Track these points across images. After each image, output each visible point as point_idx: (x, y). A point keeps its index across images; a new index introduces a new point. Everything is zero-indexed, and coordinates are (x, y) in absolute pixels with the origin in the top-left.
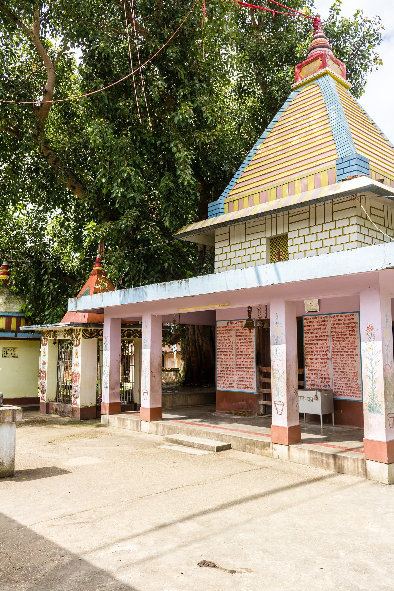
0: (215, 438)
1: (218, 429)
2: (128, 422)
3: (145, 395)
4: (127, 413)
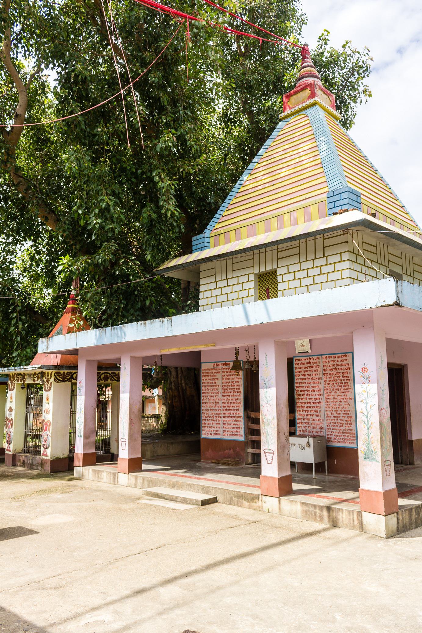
1: (203, 481)
2: (104, 475)
3: (123, 444)
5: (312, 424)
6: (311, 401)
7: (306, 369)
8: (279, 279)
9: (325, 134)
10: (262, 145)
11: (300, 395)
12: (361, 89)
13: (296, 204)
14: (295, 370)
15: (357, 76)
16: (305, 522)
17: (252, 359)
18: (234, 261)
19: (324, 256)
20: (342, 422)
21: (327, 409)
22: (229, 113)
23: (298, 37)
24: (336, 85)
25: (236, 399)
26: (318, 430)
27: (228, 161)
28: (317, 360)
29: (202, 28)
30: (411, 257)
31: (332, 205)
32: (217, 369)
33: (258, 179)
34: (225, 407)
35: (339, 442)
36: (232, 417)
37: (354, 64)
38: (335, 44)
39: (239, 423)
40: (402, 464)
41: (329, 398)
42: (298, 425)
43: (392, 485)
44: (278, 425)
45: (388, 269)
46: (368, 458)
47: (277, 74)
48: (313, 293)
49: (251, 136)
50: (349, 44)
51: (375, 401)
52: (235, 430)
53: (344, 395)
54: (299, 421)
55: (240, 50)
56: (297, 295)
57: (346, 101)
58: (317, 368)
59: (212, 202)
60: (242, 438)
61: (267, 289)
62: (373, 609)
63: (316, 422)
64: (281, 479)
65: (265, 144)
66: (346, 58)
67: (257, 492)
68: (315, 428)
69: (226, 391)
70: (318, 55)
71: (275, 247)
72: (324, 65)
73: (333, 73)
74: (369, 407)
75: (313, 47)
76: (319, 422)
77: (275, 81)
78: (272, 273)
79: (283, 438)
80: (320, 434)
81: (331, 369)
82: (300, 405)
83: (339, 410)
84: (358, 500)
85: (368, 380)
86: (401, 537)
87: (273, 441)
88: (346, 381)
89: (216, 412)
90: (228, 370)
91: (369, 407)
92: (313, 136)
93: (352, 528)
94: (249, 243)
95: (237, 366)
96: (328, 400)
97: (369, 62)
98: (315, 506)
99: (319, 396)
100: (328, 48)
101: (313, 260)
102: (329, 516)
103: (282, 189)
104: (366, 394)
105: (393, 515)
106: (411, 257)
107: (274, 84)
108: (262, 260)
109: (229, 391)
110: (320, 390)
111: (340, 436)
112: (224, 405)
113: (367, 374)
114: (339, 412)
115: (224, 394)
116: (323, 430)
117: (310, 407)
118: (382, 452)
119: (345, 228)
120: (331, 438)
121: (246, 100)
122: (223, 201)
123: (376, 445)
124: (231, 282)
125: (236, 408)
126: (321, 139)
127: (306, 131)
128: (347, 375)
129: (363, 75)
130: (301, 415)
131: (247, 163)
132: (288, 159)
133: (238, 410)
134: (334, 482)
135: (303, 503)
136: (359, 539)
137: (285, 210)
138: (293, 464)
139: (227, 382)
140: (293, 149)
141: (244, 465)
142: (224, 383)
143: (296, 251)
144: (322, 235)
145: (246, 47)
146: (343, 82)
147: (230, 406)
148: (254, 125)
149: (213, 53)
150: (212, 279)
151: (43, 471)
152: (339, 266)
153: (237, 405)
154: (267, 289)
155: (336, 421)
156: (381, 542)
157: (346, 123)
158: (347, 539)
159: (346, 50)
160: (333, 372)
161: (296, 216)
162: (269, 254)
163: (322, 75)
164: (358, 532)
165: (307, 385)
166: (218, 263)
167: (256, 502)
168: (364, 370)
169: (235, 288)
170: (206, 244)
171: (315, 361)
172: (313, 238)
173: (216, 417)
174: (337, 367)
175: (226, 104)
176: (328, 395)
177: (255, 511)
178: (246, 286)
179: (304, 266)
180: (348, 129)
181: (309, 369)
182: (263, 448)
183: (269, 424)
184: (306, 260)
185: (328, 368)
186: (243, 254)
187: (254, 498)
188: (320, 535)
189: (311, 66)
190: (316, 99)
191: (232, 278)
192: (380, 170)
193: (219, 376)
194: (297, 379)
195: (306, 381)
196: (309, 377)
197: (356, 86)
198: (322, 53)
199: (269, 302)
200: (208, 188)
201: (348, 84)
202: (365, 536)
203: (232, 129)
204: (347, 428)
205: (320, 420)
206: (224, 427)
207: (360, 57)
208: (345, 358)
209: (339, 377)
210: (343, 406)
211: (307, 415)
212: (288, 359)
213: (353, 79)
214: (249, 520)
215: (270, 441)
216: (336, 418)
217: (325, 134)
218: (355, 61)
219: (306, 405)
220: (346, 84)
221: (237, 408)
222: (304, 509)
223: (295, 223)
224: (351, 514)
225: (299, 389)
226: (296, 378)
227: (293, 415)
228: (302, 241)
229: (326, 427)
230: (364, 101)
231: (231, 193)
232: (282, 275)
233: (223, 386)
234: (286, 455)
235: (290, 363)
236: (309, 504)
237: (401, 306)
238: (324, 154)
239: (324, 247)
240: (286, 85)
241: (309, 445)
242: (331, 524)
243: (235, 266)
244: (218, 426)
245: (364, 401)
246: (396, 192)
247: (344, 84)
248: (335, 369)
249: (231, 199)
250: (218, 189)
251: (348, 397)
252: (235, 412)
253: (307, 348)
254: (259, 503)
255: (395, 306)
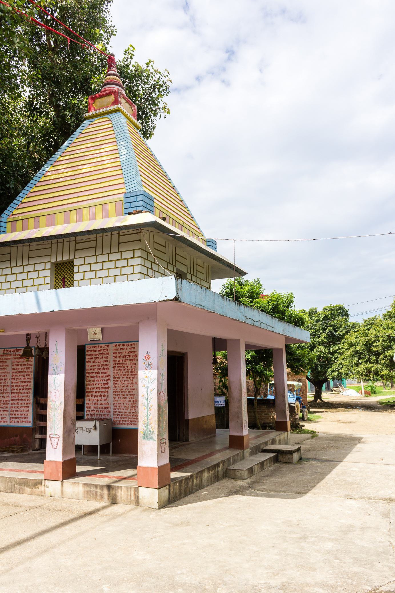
5: (100, 408)
6: (100, 386)
7: (97, 356)
8: (76, 269)
9: (125, 139)
10: (66, 139)
11: (90, 381)
12: (161, 105)
13: (95, 200)
14: (87, 357)
15: (157, 93)
16: (86, 502)
17: (42, 346)
18: (32, 248)
19: (119, 252)
20: (128, 405)
21: (115, 394)
22: (35, 102)
23: (106, 45)
24: (139, 97)
25: (26, 386)
26: (105, 413)
27: (31, 149)
28: (108, 348)
29: (8, 13)
30: (195, 259)
31: (128, 205)
32: (7, 355)
33: (60, 171)
34: (14, 393)
35: (124, 424)
36: (21, 404)
37: (155, 82)
38: (139, 60)
39: (27, 409)
40: (179, 441)
41: (117, 384)
42: (86, 409)
43: (166, 460)
44: (65, 410)
45: (175, 268)
46: (147, 437)
47: (84, 75)
48: (18, 294)
49: (57, 128)
50: (152, 63)
51: (154, 385)
52: (23, 416)
53: (131, 380)
54: (88, 406)
55: (50, 44)
56: (155, 278)
57: (148, 113)
58: (107, 356)
59: (11, 187)
60: (30, 425)
61: (64, 278)
62: (138, 575)
63: (103, 406)
64: (65, 463)
65: (69, 139)
66: (149, 75)
67: (40, 477)
68: (103, 411)
69: (16, 377)
70: (124, 66)
71: (73, 239)
72: (131, 77)
73: (137, 86)
74: (149, 391)
75: (119, 57)
76: (107, 406)
77: (83, 81)
78: (69, 263)
79: (69, 423)
80: (107, 417)
81: (120, 357)
82: (90, 390)
83: (125, 394)
84: (136, 477)
85: (150, 366)
86: (171, 507)
87: (59, 426)
88: (133, 368)
89: (4, 399)
90: (19, 357)
91: (149, 391)
92: (114, 140)
93: (129, 503)
94: (47, 232)
95: (27, 353)
96: (116, 385)
97: (168, 83)
98: (96, 486)
99: (108, 382)
100: (133, 62)
101: (108, 254)
102: (109, 494)
103: (82, 184)
104: (147, 379)
105: (165, 488)
106: (195, 259)
107: (82, 84)
108: (20, 254)
109: (19, 377)
110: (109, 376)
111: (125, 418)
112: (13, 391)
113: (149, 361)
114: (125, 396)
115: (13, 381)
116: (110, 414)
117: (99, 392)
118: (159, 432)
119: (139, 228)
120: (116, 421)
121: (53, 93)
122: (23, 188)
123: (154, 426)
124: (27, 268)
125: (25, 395)
126: (122, 143)
127: (108, 133)
128: (134, 362)
129: (163, 93)
130: (90, 400)
131: (51, 154)
132: (90, 157)
133: (27, 396)
134: (116, 462)
135: (85, 484)
136: (134, 512)
137: (85, 204)
138: (78, 448)
139: (17, 369)
140: (95, 148)
141: (31, 451)
142: (14, 369)
143: (93, 244)
144: (117, 232)
145: (55, 42)
146: (146, 96)
147: (19, 393)
148: (60, 119)
149: (18, 40)
150: (7, 265)
152: (132, 262)
153: (26, 391)
154: (64, 278)
155: (122, 405)
156: (154, 513)
157: (146, 133)
158: (124, 514)
159: (149, 68)
160: (122, 359)
161: (94, 212)
162: (66, 245)
163: (127, 85)
164: (134, 506)
165: (97, 371)
166: (14, 249)
167: (38, 488)
168: (147, 357)
169: (31, 275)
170: (2, 229)
171: (105, 348)
172: (110, 233)
173: (4, 404)
174: (126, 355)
175: (33, 92)
176: (116, 381)
177: (37, 497)
178: (42, 274)
179: (100, 258)
180: (148, 138)
181: (100, 356)
182: (48, 433)
183: (56, 409)
184: (102, 254)
185: (118, 355)
186: (41, 242)
187: (37, 483)
188: (99, 513)
189: (116, 75)
190: (119, 106)
191: (28, 264)
192: (173, 180)
193: (9, 362)
194: (88, 366)
195: (97, 367)
196: (99, 364)
197: (156, 102)
198: (128, 66)
199: (61, 291)
200: (8, 173)
201: (150, 99)
202: (140, 509)
203: (37, 118)
204: (132, 411)
205: (108, 404)
206: (11, 414)
207: (161, 77)
208: (133, 346)
209: (127, 364)
210: (130, 390)
211: (96, 400)
212: (78, 346)
213: (153, 95)
214: (28, 507)
215: (56, 426)
216: (122, 402)
217: (125, 139)
218: (156, 79)
219: (95, 390)
220: (148, 98)
221: (27, 395)
222: (86, 489)
223: (93, 218)
224: (129, 490)
225: (90, 375)
226: (87, 364)
227: (83, 400)
228: (99, 235)
229: (113, 410)
230: (163, 117)
231: (32, 181)
232: (79, 265)
233: (12, 372)
234: (71, 439)
235: (81, 351)
236: (91, 484)
237: (180, 302)
238: (123, 158)
239: (119, 243)
240: (93, 87)
241: (95, 428)
242: (110, 501)
243: (32, 254)
244: (5, 413)
245: (146, 386)
246: (186, 201)
247: (146, 97)
248: (124, 356)
249: (32, 188)
250: (19, 175)
251: (134, 382)
252: (24, 398)
253: (99, 336)
254: (42, 488)
255: (175, 301)
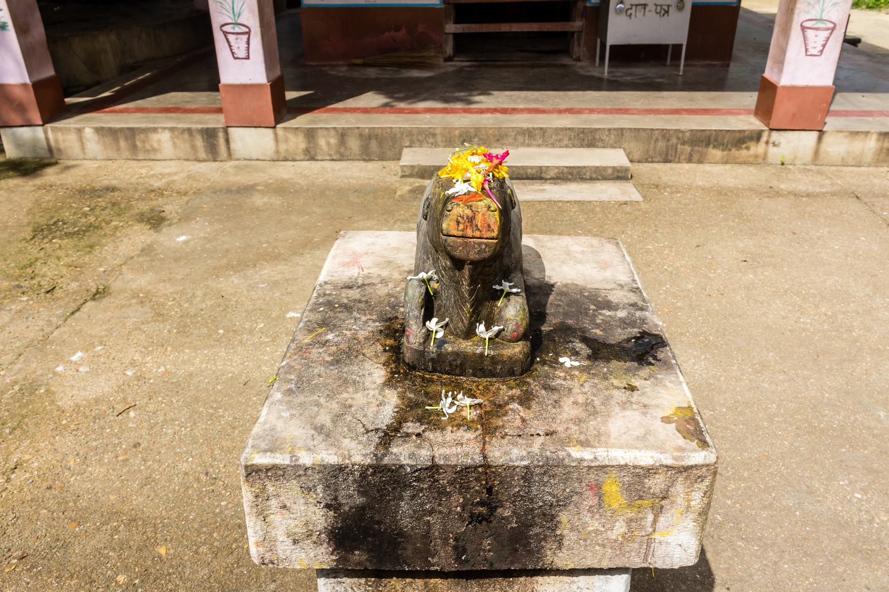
0: (566, 142)
1: (348, 116)
2: (163, 140)
3: (463, 28)
4: (122, 111)
151: (466, 170)
